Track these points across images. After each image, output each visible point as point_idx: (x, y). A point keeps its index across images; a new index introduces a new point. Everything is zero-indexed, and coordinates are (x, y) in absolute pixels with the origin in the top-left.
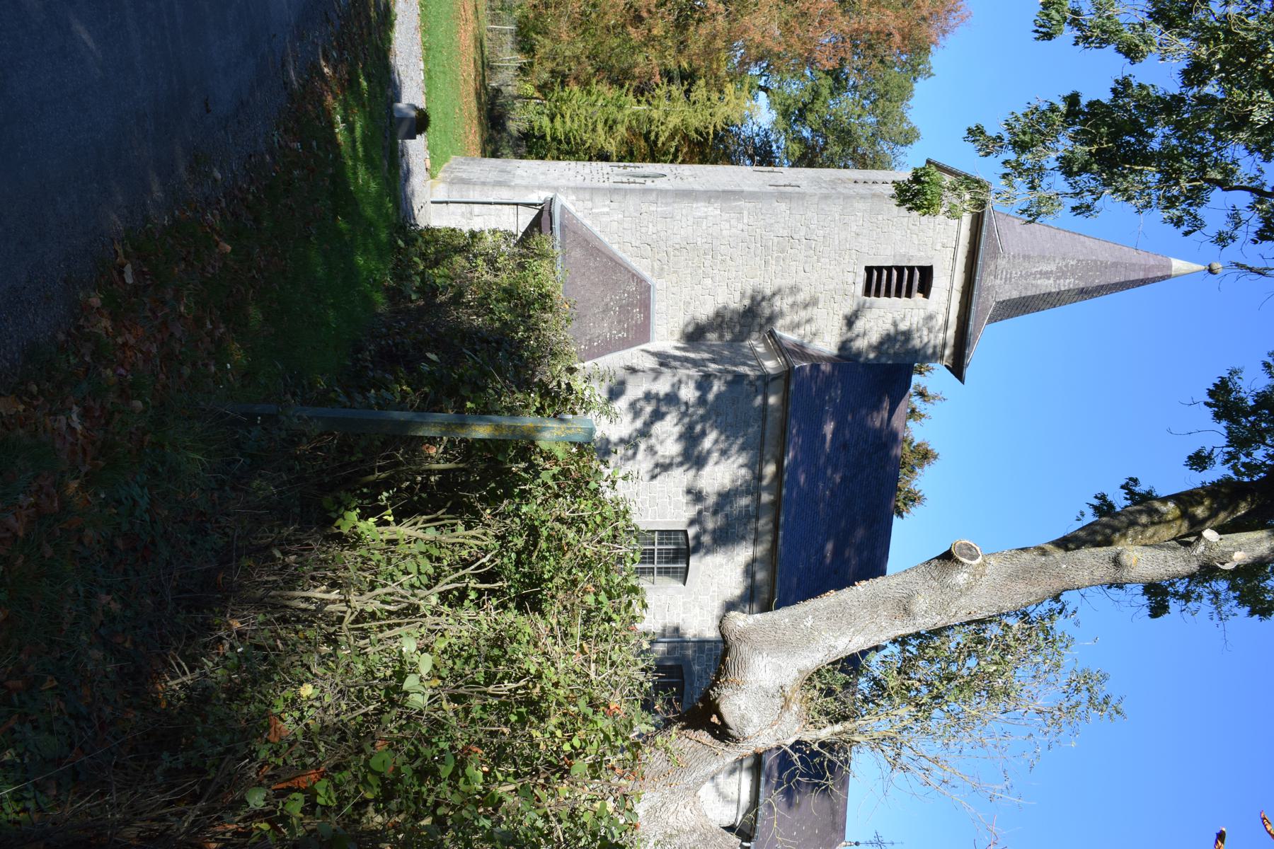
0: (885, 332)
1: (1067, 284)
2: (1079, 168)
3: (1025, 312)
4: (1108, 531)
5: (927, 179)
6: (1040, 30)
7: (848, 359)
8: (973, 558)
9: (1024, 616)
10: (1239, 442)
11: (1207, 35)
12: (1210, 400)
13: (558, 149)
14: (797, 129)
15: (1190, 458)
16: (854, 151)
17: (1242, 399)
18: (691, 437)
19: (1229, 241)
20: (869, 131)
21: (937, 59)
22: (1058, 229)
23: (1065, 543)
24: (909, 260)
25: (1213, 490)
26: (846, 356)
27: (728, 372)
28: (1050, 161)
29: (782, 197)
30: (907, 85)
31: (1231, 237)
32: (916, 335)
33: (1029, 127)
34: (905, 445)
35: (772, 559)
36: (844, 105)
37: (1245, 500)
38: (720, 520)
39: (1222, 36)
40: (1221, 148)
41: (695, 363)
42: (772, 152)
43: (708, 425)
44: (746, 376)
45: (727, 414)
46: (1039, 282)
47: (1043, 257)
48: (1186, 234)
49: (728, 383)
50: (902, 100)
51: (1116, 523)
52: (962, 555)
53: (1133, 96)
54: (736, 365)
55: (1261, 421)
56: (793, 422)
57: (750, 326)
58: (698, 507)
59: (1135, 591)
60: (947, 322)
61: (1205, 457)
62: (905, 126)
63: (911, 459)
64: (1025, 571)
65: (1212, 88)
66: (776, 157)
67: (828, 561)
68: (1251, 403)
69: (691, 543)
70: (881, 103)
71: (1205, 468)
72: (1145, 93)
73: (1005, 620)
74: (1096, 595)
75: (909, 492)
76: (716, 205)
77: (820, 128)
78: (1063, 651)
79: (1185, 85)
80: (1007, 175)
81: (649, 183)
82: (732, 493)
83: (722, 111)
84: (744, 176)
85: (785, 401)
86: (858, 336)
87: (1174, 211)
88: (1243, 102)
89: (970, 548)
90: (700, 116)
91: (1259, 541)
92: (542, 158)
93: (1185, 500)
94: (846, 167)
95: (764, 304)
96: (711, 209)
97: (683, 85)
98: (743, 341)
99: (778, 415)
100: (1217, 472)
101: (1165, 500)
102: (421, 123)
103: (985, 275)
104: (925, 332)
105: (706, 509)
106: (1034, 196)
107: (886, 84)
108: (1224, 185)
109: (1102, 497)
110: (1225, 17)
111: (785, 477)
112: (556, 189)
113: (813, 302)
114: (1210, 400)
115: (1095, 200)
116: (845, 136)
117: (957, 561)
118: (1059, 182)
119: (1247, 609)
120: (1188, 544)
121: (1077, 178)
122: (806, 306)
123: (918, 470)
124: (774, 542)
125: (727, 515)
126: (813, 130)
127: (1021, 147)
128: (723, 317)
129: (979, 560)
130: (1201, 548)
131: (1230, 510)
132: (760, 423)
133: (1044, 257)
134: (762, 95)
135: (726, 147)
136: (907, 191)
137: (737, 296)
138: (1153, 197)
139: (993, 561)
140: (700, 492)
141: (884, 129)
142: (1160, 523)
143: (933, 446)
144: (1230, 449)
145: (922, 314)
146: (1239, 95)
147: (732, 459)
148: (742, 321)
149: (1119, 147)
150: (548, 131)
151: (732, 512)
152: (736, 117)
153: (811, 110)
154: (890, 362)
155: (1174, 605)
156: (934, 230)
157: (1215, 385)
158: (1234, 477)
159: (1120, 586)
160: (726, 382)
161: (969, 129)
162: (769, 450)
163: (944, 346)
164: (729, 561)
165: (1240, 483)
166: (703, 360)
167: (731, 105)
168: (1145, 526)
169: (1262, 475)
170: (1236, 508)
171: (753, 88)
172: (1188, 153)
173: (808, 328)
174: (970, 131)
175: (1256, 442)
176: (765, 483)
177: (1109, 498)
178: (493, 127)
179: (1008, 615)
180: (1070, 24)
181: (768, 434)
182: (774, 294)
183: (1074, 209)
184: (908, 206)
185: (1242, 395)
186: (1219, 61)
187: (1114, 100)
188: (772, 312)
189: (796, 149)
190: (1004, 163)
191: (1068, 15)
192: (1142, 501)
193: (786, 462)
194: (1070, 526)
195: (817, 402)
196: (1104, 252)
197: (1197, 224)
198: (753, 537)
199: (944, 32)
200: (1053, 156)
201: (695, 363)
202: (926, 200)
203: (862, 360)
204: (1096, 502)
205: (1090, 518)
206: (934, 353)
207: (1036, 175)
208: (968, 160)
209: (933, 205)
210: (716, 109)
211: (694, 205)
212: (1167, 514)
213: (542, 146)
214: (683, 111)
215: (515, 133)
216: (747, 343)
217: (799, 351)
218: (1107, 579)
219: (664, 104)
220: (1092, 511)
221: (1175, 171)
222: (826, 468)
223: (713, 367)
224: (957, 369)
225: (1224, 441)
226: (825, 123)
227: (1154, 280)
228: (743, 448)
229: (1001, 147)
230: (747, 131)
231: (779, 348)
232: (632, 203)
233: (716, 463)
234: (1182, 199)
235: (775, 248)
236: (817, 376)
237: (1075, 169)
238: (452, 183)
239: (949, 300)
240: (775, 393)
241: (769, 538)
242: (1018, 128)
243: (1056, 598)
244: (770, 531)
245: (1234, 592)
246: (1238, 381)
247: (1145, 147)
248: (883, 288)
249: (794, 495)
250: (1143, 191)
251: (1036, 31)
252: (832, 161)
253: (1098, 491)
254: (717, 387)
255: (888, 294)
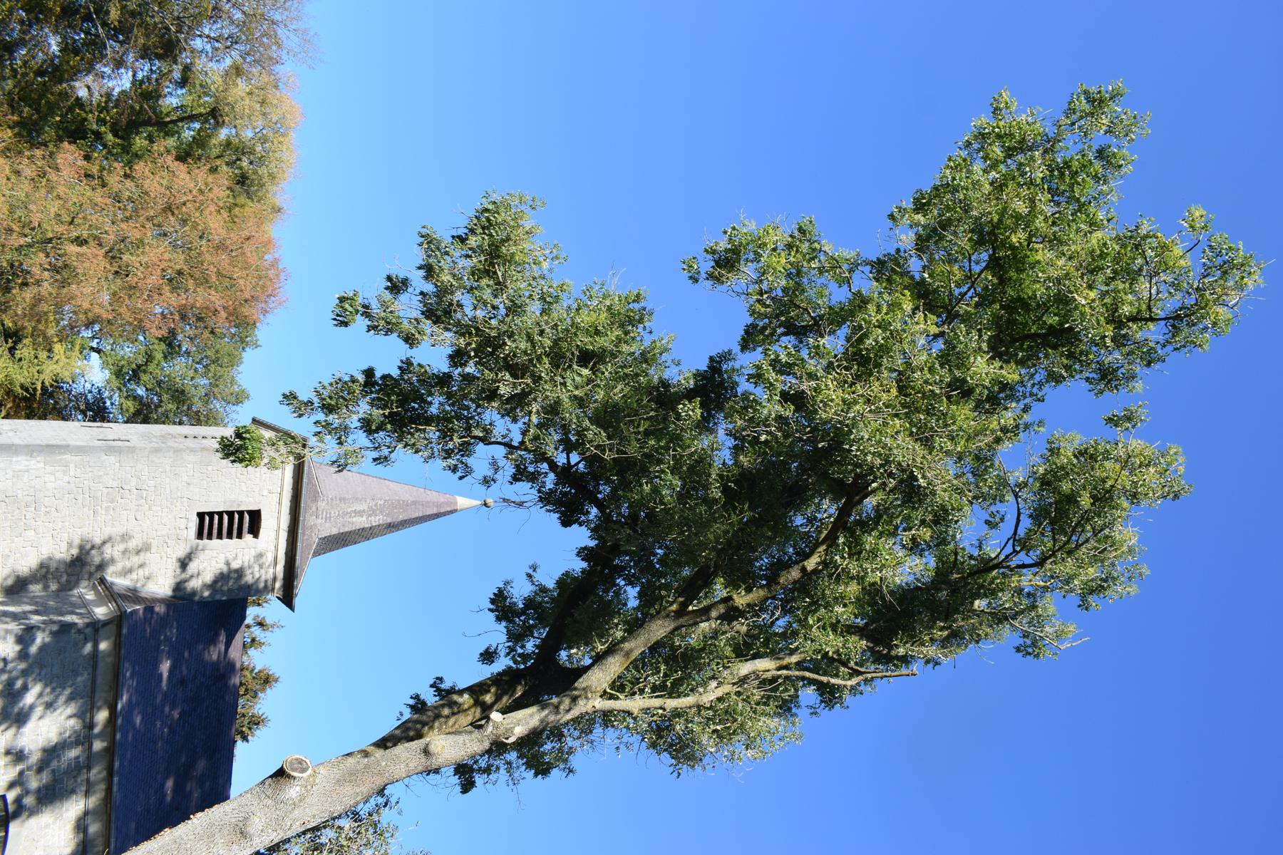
0: (218, 572)
1: (378, 520)
2: (377, 427)
3: (344, 546)
4: (419, 726)
5: (248, 436)
6: (338, 318)
7: (182, 598)
8: (304, 770)
9: (356, 816)
10: (516, 637)
11: (463, 330)
12: (492, 607)
14: (132, 387)
15: (481, 654)
16: (188, 409)
17: (515, 604)
18: (9, 694)
19: (492, 483)
20: (203, 392)
21: (262, 333)
22: (368, 475)
23: (383, 744)
24: (239, 505)
25: (497, 679)
27: (53, 622)
28: (354, 421)
29: (110, 450)
30: (236, 353)
31: (493, 480)
32: (248, 572)
33: (335, 394)
34: (247, 673)
35: (107, 809)
36: (177, 368)
37: (520, 684)
38: (45, 777)
39: (474, 332)
40: (480, 413)
41: (15, 617)
42: (106, 408)
43: (30, 679)
44: (74, 624)
45: (53, 665)
46: (354, 519)
48: (461, 478)
49: (52, 633)
50: (232, 366)
51: (424, 718)
52: (293, 770)
53: (414, 373)
54: (62, 614)
55: (530, 619)
56: (127, 665)
57: (78, 575)
58: (19, 768)
59: (448, 774)
60: (276, 559)
61: (493, 653)
62: (236, 389)
63: (253, 685)
64: (351, 774)
65: (471, 369)
66: (111, 413)
67: (169, 798)
68: (521, 606)
69: (11, 808)
70: (212, 368)
71: (493, 662)
72: (423, 370)
73: (338, 823)
74: (418, 783)
75: (253, 716)
76: (38, 459)
77: (154, 388)
78: (389, 840)
79: (452, 366)
80: (320, 433)
82: (59, 747)
83: (49, 371)
84: (75, 431)
85: (117, 646)
86: (192, 576)
87: (451, 461)
88: (492, 380)
89: (300, 762)
90: (26, 373)
91: (531, 715)
93: (476, 690)
94: (181, 423)
95: (93, 552)
96: (33, 462)
97: (7, 343)
98: (70, 590)
99: (110, 660)
100: (502, 663)
101: (461, 692)
103: (307, 516)
104: (257, 568)
105: (29, 768)
106: (342, 450)
107: (217, 352)
108: (485, 440)
109: (417, 697)
110: (475, 318)
111: (119, 721)
113: (146, 548)
114: (492, 607)
115: (390, 452)
116: (179, 396)
117: (289, 776)
118: (361, 439)
119: (533, 771)
120: (480, 727)
121: (376, 435)
122: (138, 552)
123: (260, 694)
124: (109, 790)
125: (53, 771)
126: (147, 390)
127: (329, 409)
128: (48, 568)
129: (310, 771)
130: (490, 729)
131: (510, 693)
132: (90, 670)
133: (357, 499)
134: (94, 355)
135: (56, 403)
136: (231, 446)
137: (64, 546)
138: (435, 450)
139: (322, 770)
140: (21, 751)
141: (216, 390)
142: (459, 712)
143: (274, 670)
144: (510, 644)
145: (253, 553)
146: (489, 375)
147: (59, 711)
148: (69, 571)
149: (406, 411)
151: (59, 766)
152: (66, 375)
153: (145, 372)
154: (224, 598)
155: (479, 779)
156: (261, 479)
157: (495, 594)
158: (514, 666)
159: (437, 771)
160: (52, 633)
161: (284, 395)
162: (100, 696)
163: (275, 579)
164: (56, 819)
165: (518, 669)
166: (25, 613)
167: (61, 364)
168: (448, 717)
169: (532, 661)
170: (514, 691)
171: (84, 349)
172: (459, 418)
174: (285, 396)
175: (527, 636)
176: (97, 730)
177: (422, 697)
179: (339, 817)
180: (362, 315)
181: (99, 680)
182: (104, 543)
183: (375, 460)
184: (231, 458)
185: (514, 600)
186: (474, 349)
187: (401, 375)
188: (103, 560)
189: (131, 406)
190: (315, 423)
191: (360, 308)
192: (446, 695)
193: (119, 706)
194: (388, 725)
195: (152, 642)
196: (405, 493)
197: (468, 471)
198: (84, 788)
199: (265, 312)
200: (355, 417)
201: (15, 617)
202: (248, 454)
204: (412, 702)
205: (407, 714)
206: (266, 586)
207: (343, 433)
208: (284, 418)
209: (254, 458)
210: (44, 367)
211: (14, 459)
212: (464, 704)
214: (7, 367)
216: (75, 592)
217: (133, 595)
218: (420, 768)
220: (409, 710)
221: (449, 430)
222: (163, 706)
223: (36, 619)
224: (288, 598)
225: (504, 638)
226: (159, 383)
227: (445, 514)
228: (71, 698)
229: (312, 410)
230: (78, 388)
231: (110, 593)
233: (40, 718)
234: (456, 451)
235: (104, 499)
236: (151, 618)
237: (374, 428)
239: (277, 539)
240: (106, 638)
241: (103, 786)
242: (326, 393)
243: (381, 792)
244: (103, 780)
245: (522, 759)
246: (511, 589)
247: (426, 412)
248: (215, 531)
249: (130, 738)
250: (427, 445)
251: (335, 319)
252: (167, 417)
253: (412, 693)
254: (40, 638)
255: (220, 536)
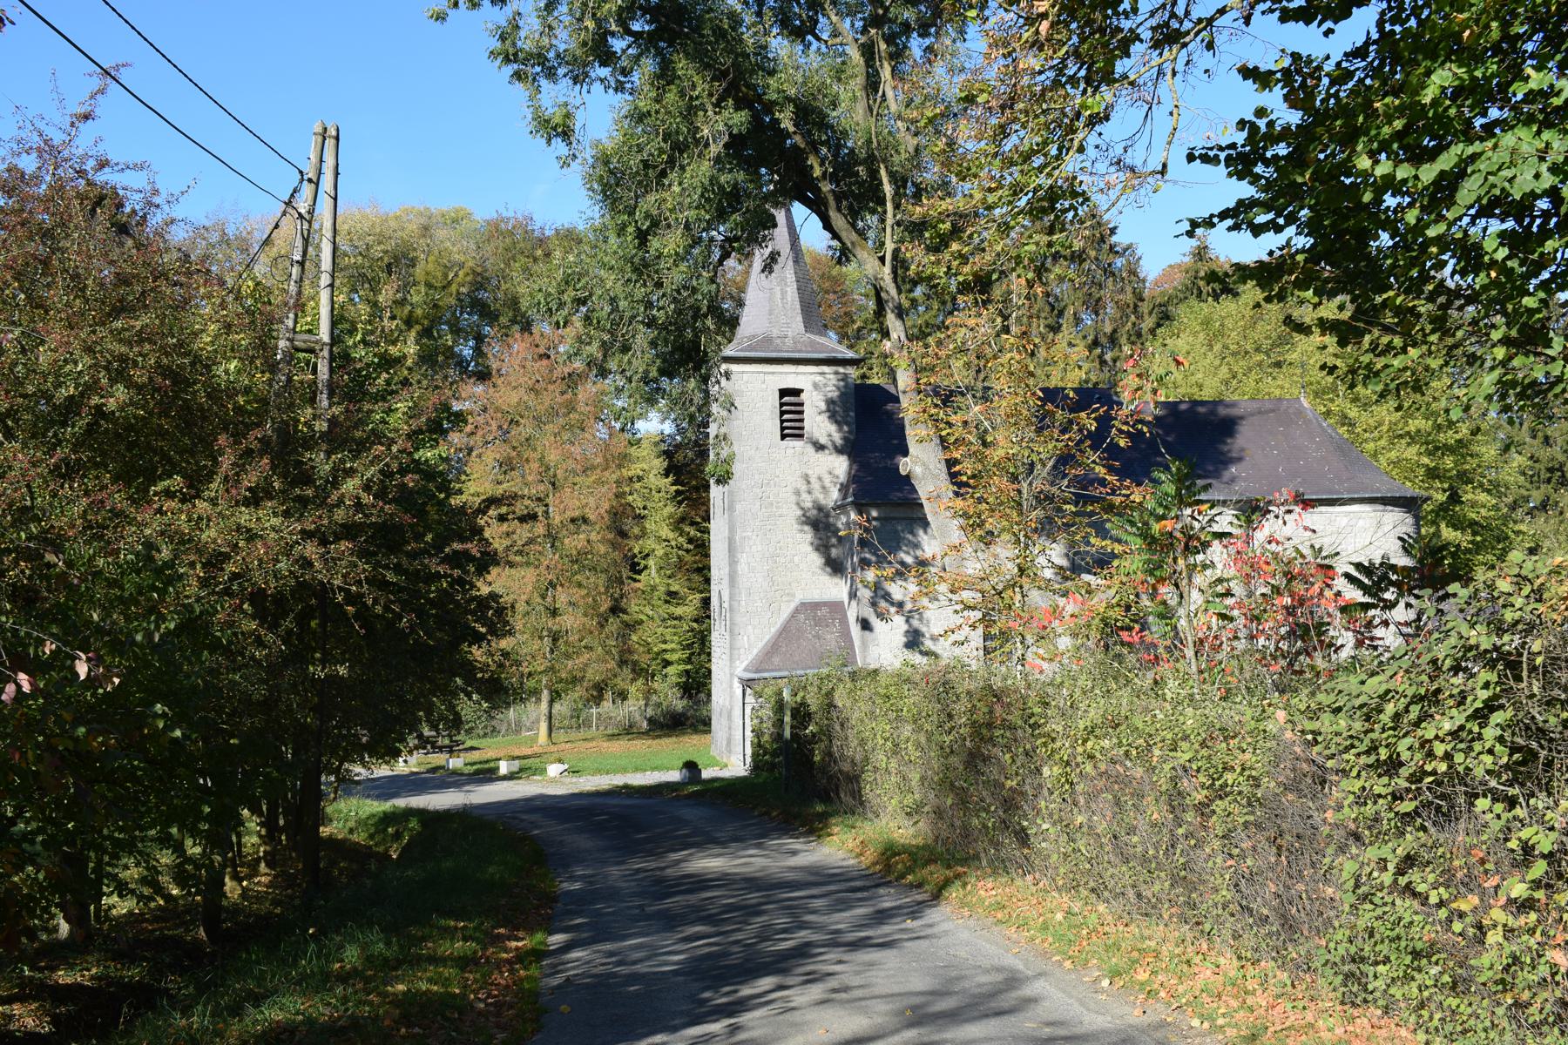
13: (699, 654)
26: (848, 449)
29: (731, 508)
32: (830, 395)
41: (854, 571)
47: (771, 299)
81: (726, 605)
92: (710, 671)
102: (691, 767)
112: (732, 675)
122: (809, 482)
145: (815, 393)
150: (681, 667)
163: (836, 373)
173: (827, 480)
178: (683, 724)
181: (902, 515)
182: (802, 509)
201: (854, 571)
203: (852, 437)
206: (842, 380)
213: (697, 672)
215: (685, 702)
219: (650, 543)
232: (738, 619)
238: (730, 752)
248: (797, 424)
255: (802, 420)
